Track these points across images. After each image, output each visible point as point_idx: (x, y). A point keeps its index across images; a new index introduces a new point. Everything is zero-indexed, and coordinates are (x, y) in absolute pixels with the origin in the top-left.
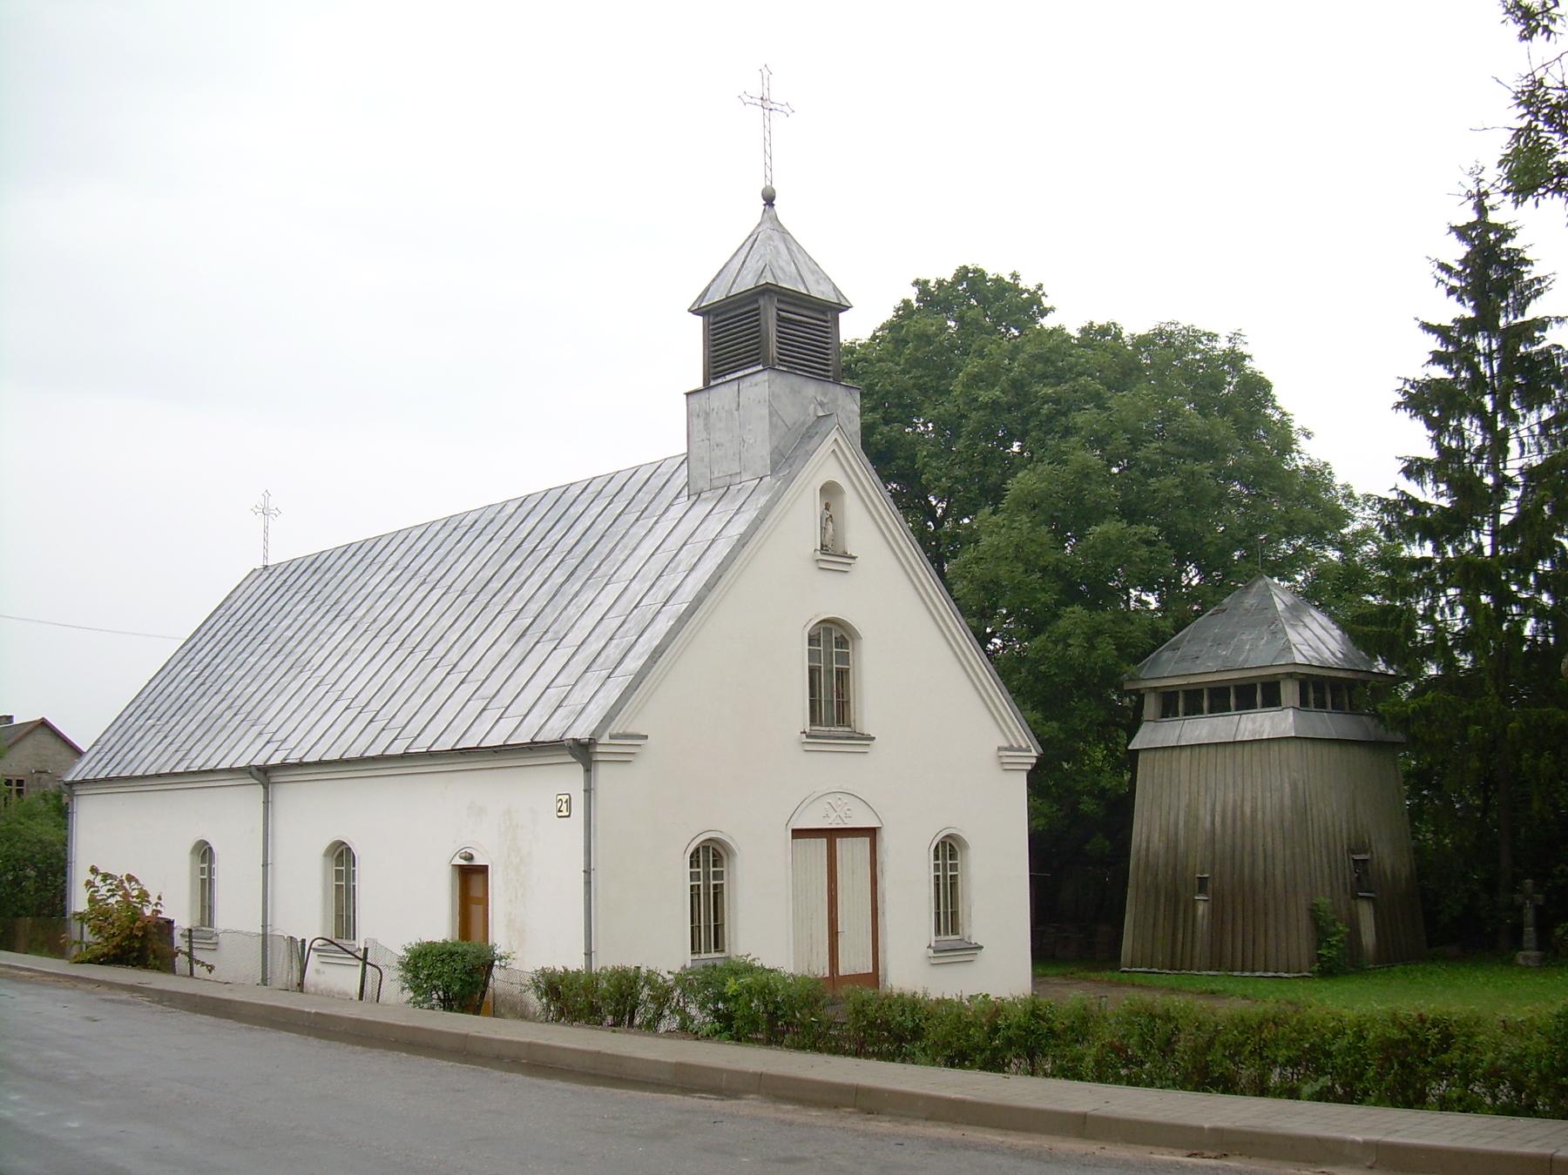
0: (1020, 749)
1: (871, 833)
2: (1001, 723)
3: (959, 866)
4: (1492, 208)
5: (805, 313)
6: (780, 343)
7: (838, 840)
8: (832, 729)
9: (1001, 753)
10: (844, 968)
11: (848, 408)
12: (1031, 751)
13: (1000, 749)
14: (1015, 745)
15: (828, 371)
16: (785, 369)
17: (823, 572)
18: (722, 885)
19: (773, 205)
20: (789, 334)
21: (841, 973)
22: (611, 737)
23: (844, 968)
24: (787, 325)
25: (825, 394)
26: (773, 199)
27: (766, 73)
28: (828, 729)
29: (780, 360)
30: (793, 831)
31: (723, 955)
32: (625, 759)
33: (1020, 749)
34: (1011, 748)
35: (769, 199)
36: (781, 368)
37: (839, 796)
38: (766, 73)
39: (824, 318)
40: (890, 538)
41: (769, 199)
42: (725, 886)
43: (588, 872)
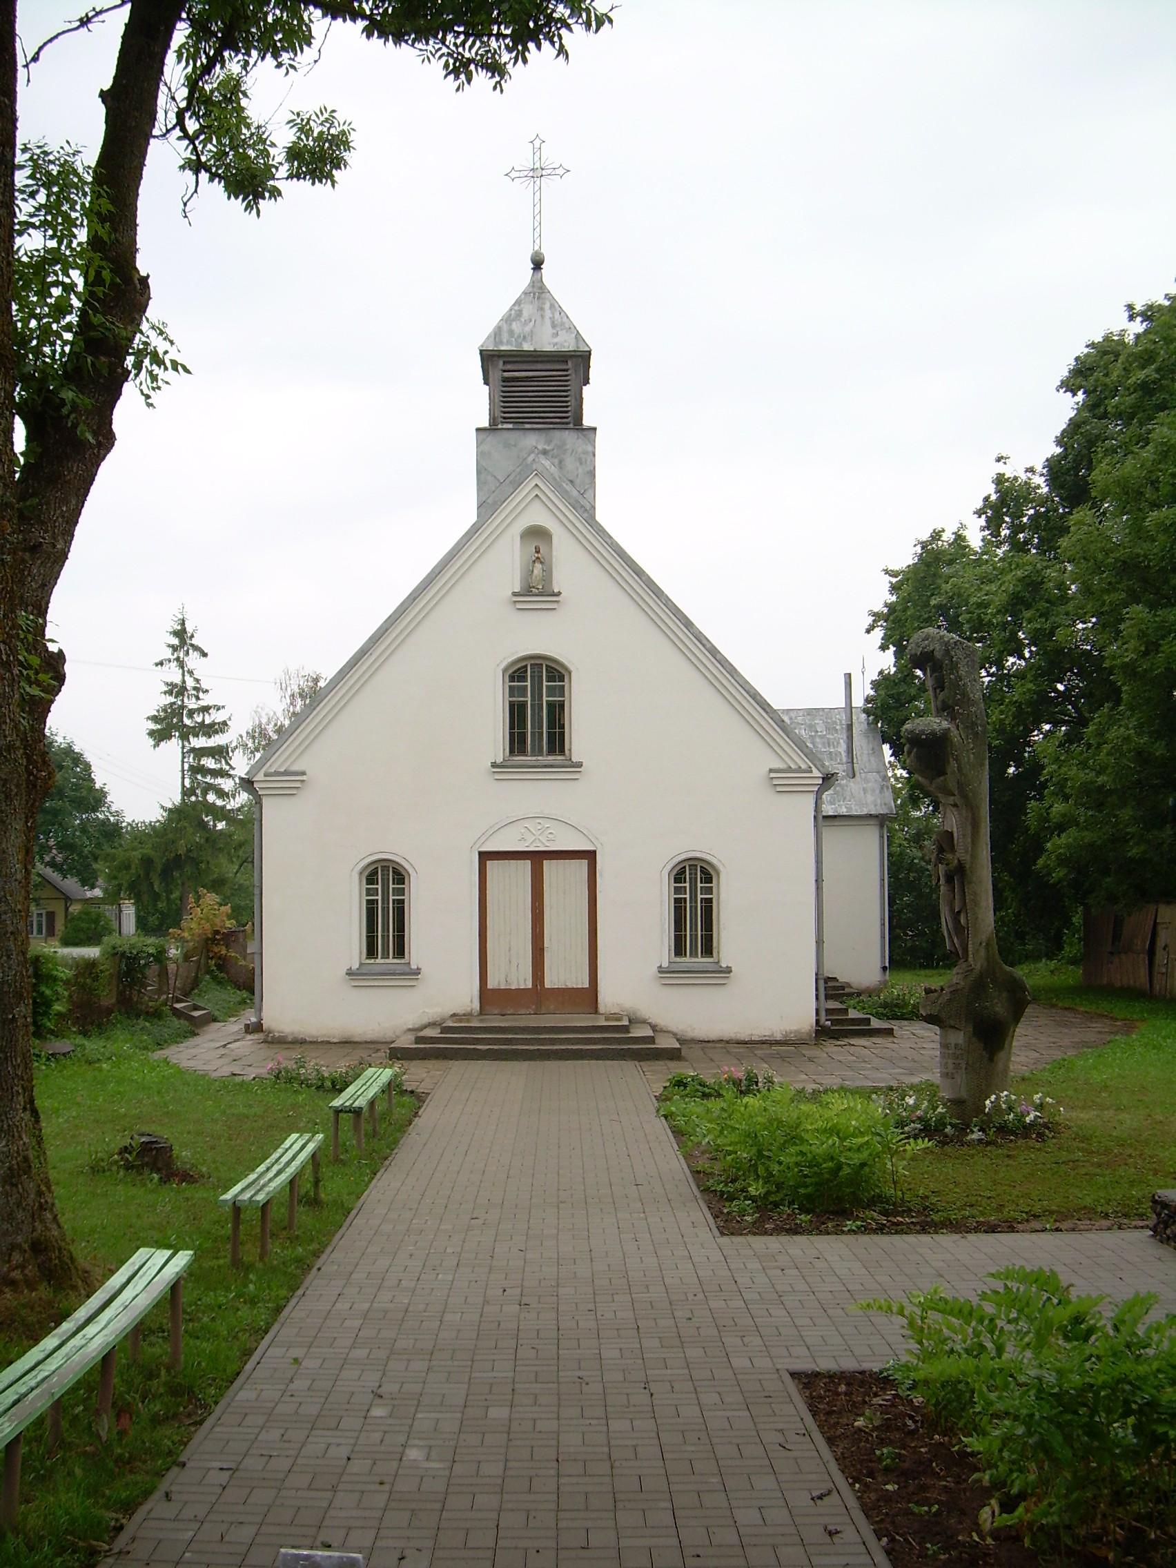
0: (799, 770)
1: (485, 857)
2: (772, 744)
3: (714, 890)
4: (29, 235)
5: (539, 366)
6: (504, 402)
7: (488, 862)
8: (540, 758)
9: (773, 775)
10: (553, 979)
11: (580, 450)
12: (811, 772)
13: (771, 771)
14: (793, 766)
15: (567, 418)
16: (510, 426)
17: (521, 612)
18: (711, 899)
19: (541, 269)
20: (533, 391)
21: (489, 986)
22: (265, 775)
23: (553, 979)
24: (513, 384)
25: (549, 442)
26: (542, 263)
27: (537, 144)
28: (534, 758)
29: (504, 418)
30: (480, 853)
31: (403, 961)
32: (289, 793)
33: (799, 770)
34: (789, 770)
35: (538, 264)
36: (505, 426)
37: (538, 821)
38: (537, 144)
39: (565, 367)
40: (607, 567)
41: (538, 264)
42: (714, 901)
43: (819, 881)
